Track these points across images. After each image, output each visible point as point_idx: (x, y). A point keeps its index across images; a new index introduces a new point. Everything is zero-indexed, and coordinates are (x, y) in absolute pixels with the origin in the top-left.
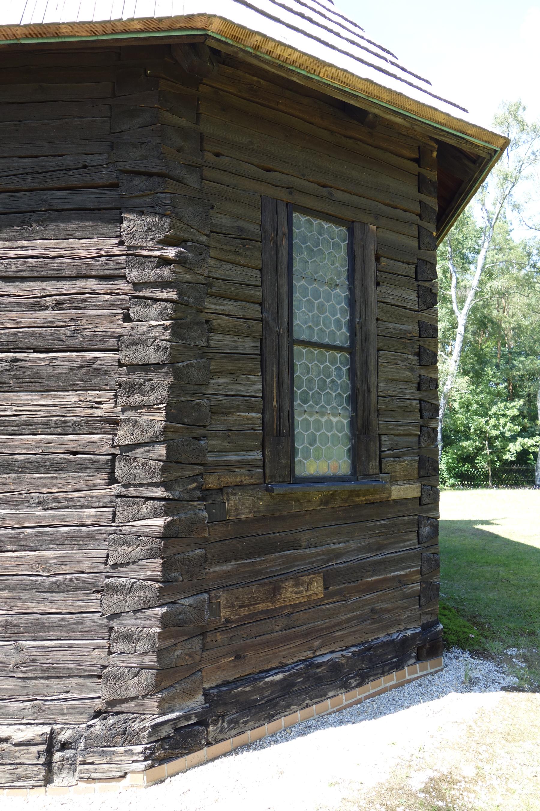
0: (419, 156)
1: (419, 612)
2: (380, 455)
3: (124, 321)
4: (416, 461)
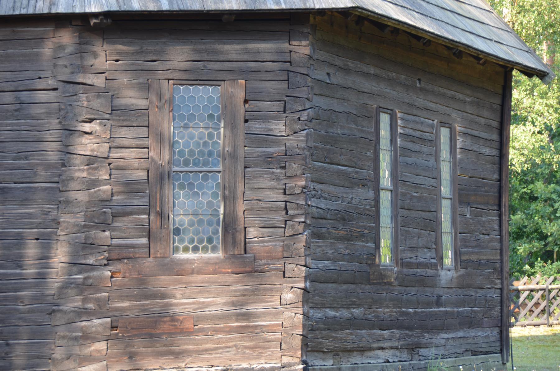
1: (281, 354)
2: (245, 241)
3: (62, 167)
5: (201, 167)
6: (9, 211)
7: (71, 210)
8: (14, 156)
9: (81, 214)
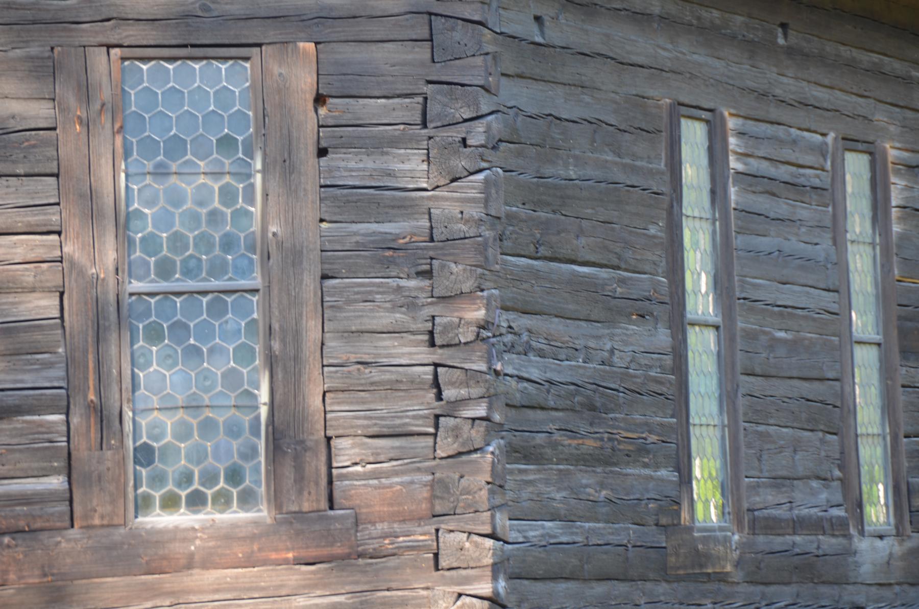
4: (425, 486)
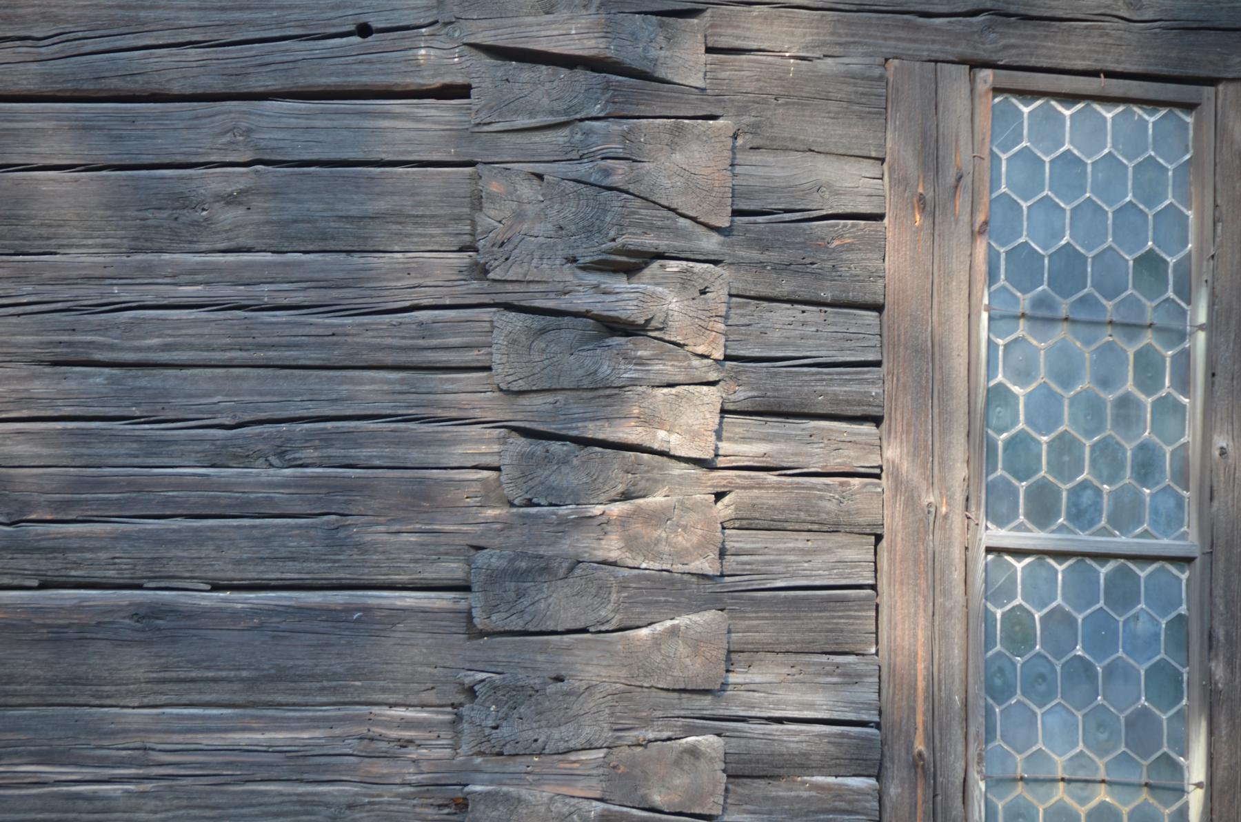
0: (880, 817)
5: (1103, 532)
6: (176, 738)
7: (530, 735)
8: (213, 441)
9: (584, 756)
